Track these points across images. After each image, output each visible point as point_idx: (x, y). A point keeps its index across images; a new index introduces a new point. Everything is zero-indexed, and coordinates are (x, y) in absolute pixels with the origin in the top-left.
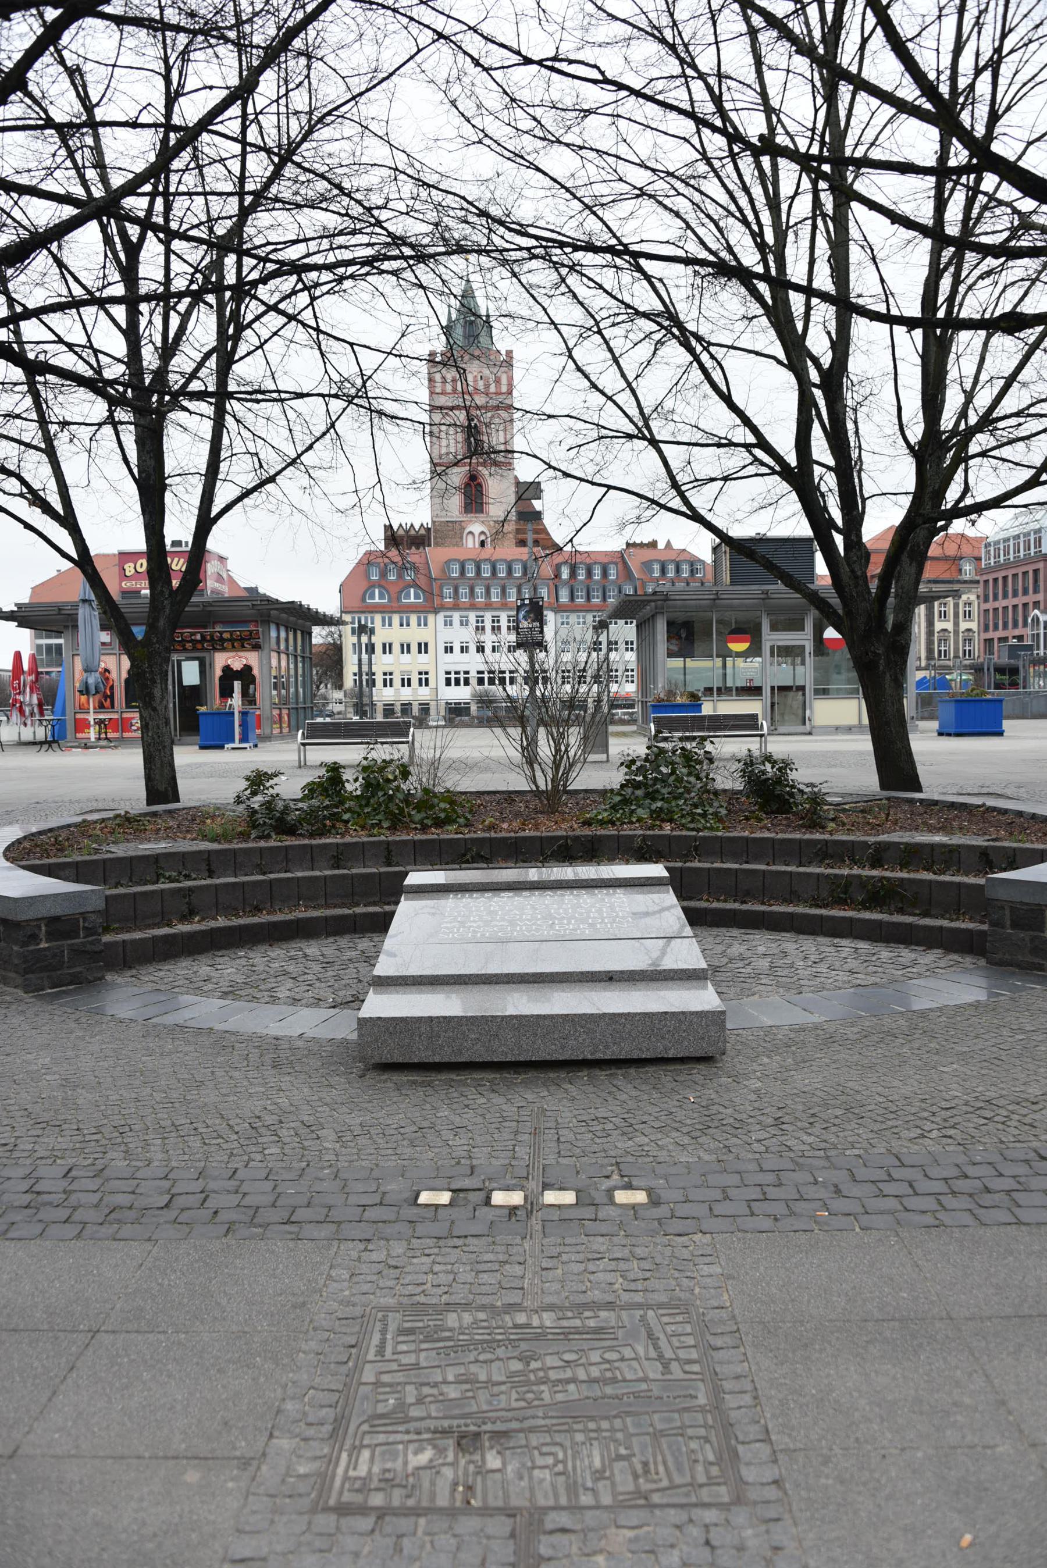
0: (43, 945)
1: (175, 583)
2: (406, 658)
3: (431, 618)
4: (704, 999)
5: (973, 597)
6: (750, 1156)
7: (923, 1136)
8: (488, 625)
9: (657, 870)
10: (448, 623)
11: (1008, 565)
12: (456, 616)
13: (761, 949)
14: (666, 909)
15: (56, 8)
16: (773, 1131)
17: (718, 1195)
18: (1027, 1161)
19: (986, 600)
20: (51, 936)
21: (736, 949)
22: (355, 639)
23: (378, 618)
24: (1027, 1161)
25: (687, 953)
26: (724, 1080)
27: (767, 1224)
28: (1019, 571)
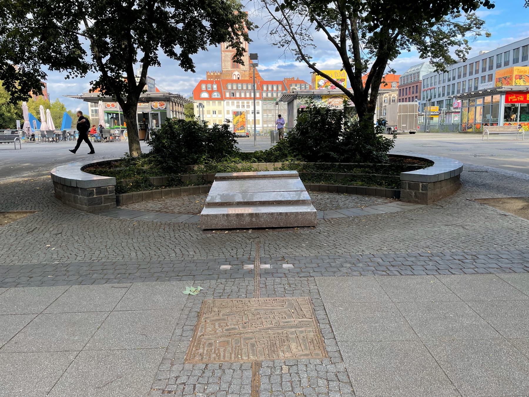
0: (95, 196)
1: (137, 84)
2: (214, 115)
3: (222, 102)
4: (310, 209)
5: (396, 95)
6: (325, 254)
7: (381, 249)
8: (240, 104)
9: (295, 172)
10: (228, 103)
11: (407, 85)
12: (230, 101)
13: (327, 197)
14: (297, 183)
15: (135, 9)
16: (333, 247)
17: (316, 265)
18: (416, 257)
19: (400, 96)
20: (97, 193)
21: (320, 197)
22: (198, 109)
23: (205, 102)
24: (416, 257)
25: (306, 195)
26: (302, 300)
27: (332, 274)
28: (411, 86)
